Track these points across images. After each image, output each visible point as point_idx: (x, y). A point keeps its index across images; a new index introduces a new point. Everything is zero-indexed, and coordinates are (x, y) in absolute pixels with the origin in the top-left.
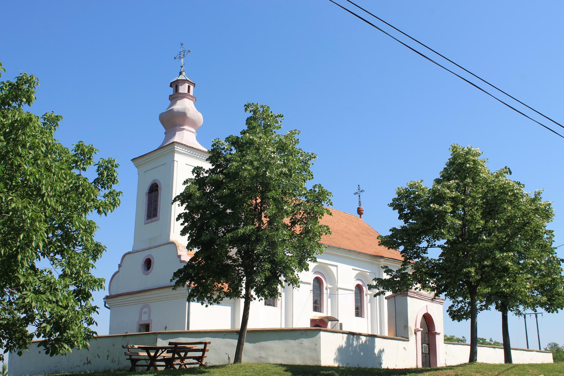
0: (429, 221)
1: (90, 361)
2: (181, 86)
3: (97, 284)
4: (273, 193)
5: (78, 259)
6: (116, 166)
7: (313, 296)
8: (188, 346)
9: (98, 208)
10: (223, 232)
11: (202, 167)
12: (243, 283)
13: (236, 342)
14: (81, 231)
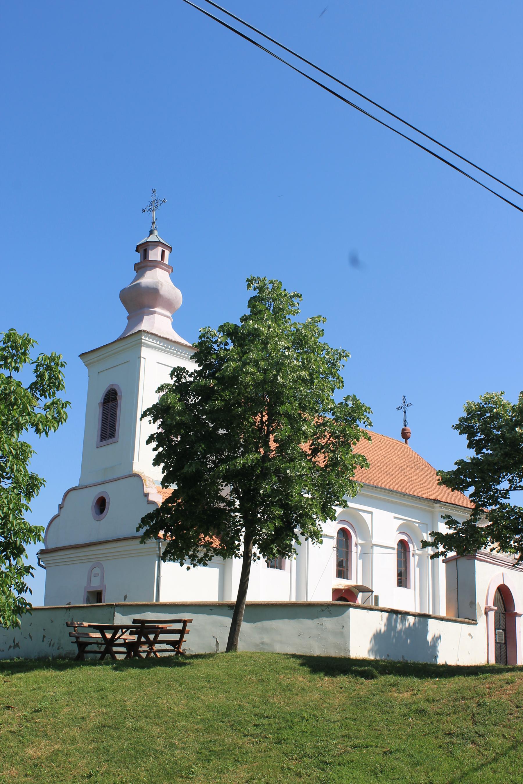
0: (513, 452)
1: (17, 644)
2: (152, 250)
3: (34, 534)
4: (287, 407)
5: (6, 498)
6: (62, 365)
7: (337, 556)
8: (161, 625)
9: (35, 425)
10: (214, 462)
11: (184, 368)
12: (241, 535)
13: (229, 621)
14: (11, 458)
